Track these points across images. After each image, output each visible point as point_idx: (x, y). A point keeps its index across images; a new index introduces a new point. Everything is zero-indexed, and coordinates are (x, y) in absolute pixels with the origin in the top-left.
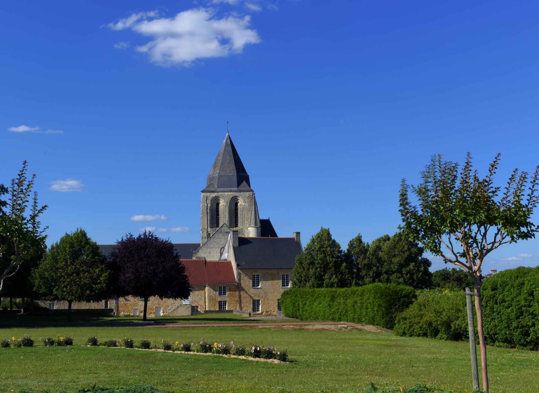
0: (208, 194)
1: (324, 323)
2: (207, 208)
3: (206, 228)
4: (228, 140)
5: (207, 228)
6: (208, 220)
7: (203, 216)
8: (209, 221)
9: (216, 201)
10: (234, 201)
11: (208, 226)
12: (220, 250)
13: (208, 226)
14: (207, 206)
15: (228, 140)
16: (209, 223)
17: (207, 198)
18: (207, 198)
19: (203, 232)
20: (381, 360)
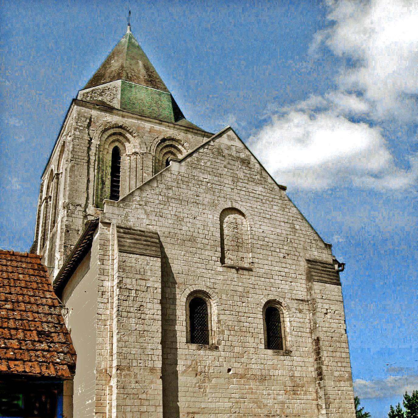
0: (94, 113)
1: (209, 314)
2: (89, 149)
3: (83, 202)
4: (299, 107)
5: (86, 206)
6: (88, 181)
7: (73, 166)
8: (91, 184)
9: (113, 141)
10: (165, 151)
11: (87, 198)
12: (217, 215)
13: (87, 198)
14: (90, 142)
15: (299, 107)
16: (91, 191)
17: (90, 120)
18: (90, 120)
19: (73, 213)
20: (220, 330)
